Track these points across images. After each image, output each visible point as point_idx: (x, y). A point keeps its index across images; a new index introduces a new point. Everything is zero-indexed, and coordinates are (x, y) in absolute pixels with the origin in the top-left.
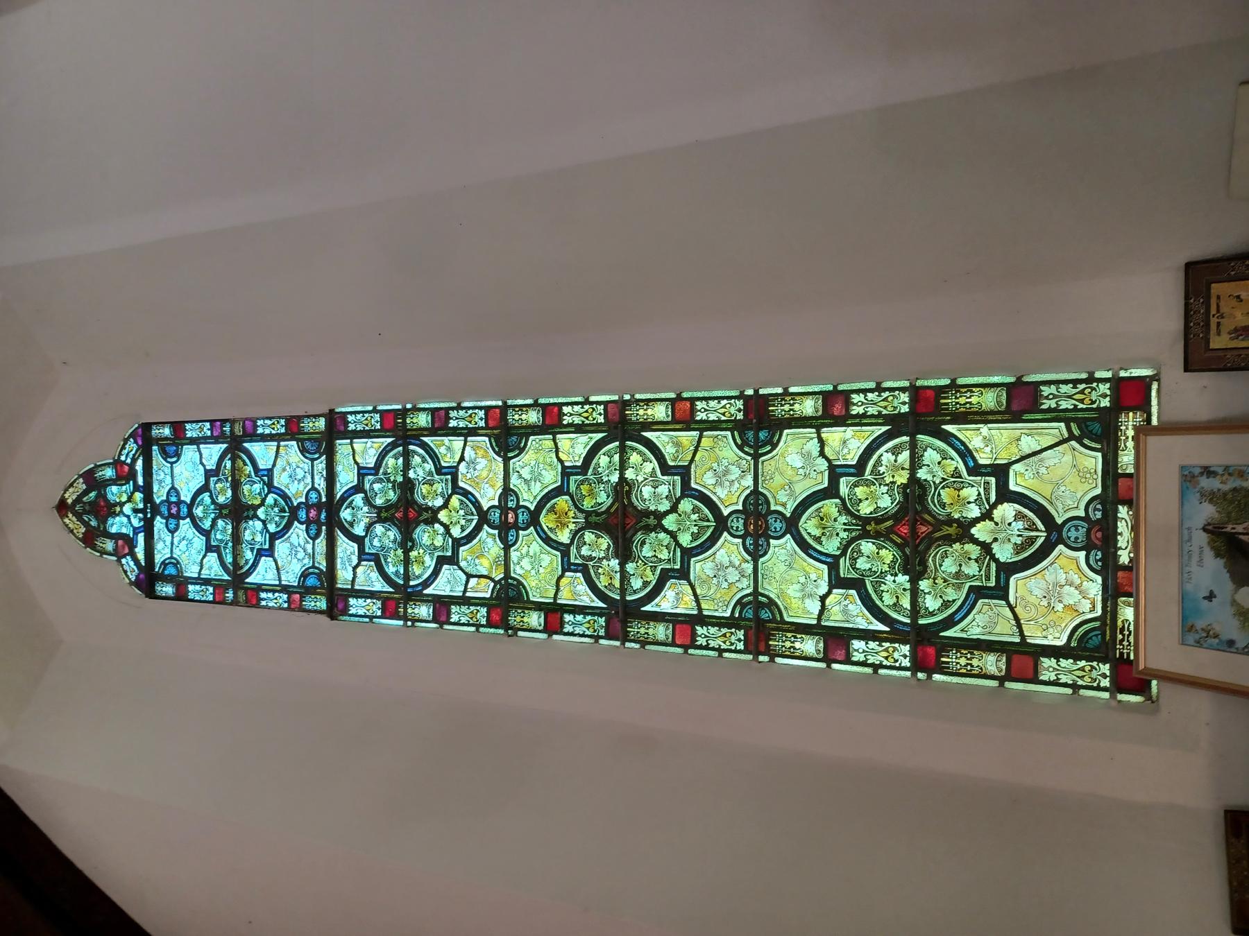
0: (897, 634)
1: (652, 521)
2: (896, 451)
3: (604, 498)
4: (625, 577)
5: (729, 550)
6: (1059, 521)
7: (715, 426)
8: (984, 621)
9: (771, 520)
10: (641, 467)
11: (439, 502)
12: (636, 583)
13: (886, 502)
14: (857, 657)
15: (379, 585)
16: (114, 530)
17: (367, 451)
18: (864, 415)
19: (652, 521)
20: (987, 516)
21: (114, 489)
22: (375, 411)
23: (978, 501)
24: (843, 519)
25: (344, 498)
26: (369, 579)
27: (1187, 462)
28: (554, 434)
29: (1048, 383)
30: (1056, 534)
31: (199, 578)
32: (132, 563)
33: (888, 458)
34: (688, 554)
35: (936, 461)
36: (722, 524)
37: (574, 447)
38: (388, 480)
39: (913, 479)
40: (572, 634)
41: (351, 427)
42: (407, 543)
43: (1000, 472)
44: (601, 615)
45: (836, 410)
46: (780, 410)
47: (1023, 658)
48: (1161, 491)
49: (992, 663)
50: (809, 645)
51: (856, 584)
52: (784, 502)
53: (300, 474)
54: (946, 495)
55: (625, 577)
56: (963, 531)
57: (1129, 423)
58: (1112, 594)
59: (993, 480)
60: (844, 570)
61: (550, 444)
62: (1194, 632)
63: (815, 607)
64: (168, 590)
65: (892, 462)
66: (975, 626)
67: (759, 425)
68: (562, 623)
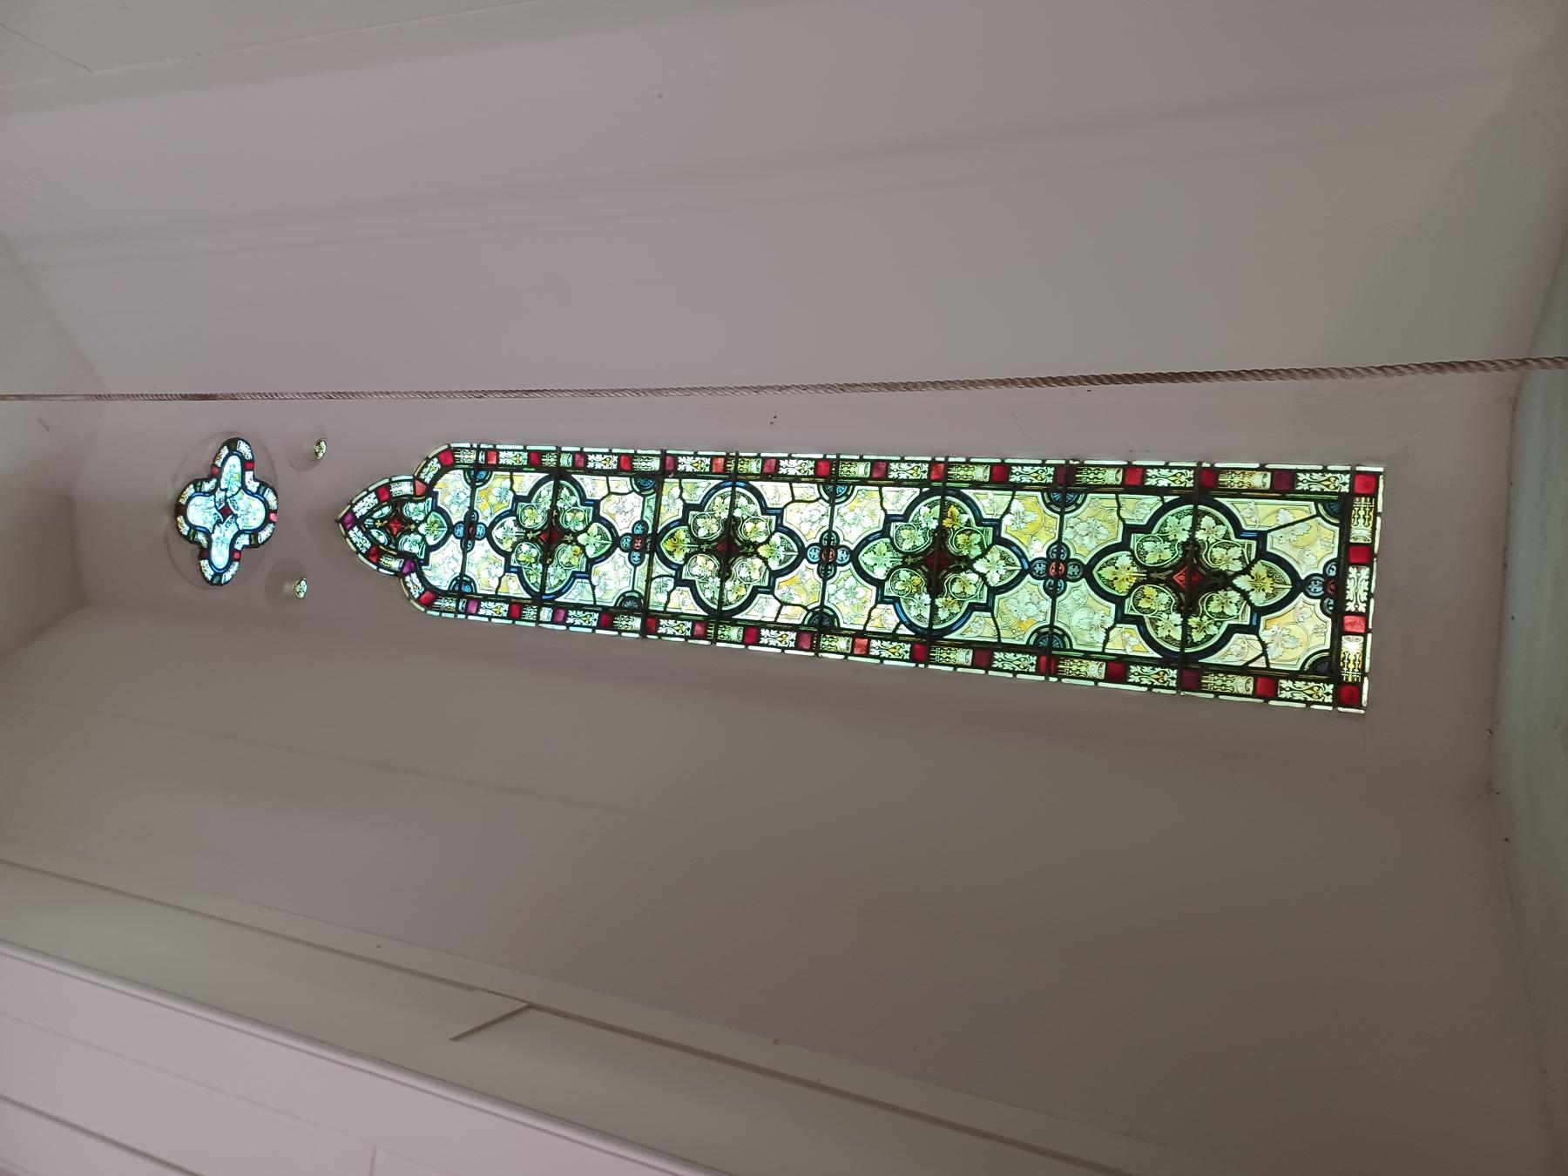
0: (1167, 659)
1: (1220, 581)
2: (931, 506)
3: (716, 530)
4: (934, 609)
5: (808, 573)
6: (1303, 577)
12: (942, 614)
14: (874, 652)
15: (691, 608)
16: (406, 548)
18: (1308, 492)
19: (909, 560)
20: (1246, 571)
21: (412, 506)
22: (525, 450)
23: (1242, 559)
26: (683, 601)
28: (880, 486)
30: (1300, 586)
31: (496, 596)
32: (417, 581)
33: (718, 500)
35: (1211, 530)
38: (1166, 539)
39: (1192, 538)
40: (767, 645)
43: (1261, 537)
46: (1086, 477)
47: (1267, 681)
50: (1095, 669)
51: (691, 584)
54: (569, 517)
55: (934, 609)
57: (1361, 505)
58: (1338, 633)
59: (1254, 543)
60: (889, 590)
61: (877, 495)
63: (495, 583)
65: (1178, 525)
67: (1065, 489)
68: (759, 636)
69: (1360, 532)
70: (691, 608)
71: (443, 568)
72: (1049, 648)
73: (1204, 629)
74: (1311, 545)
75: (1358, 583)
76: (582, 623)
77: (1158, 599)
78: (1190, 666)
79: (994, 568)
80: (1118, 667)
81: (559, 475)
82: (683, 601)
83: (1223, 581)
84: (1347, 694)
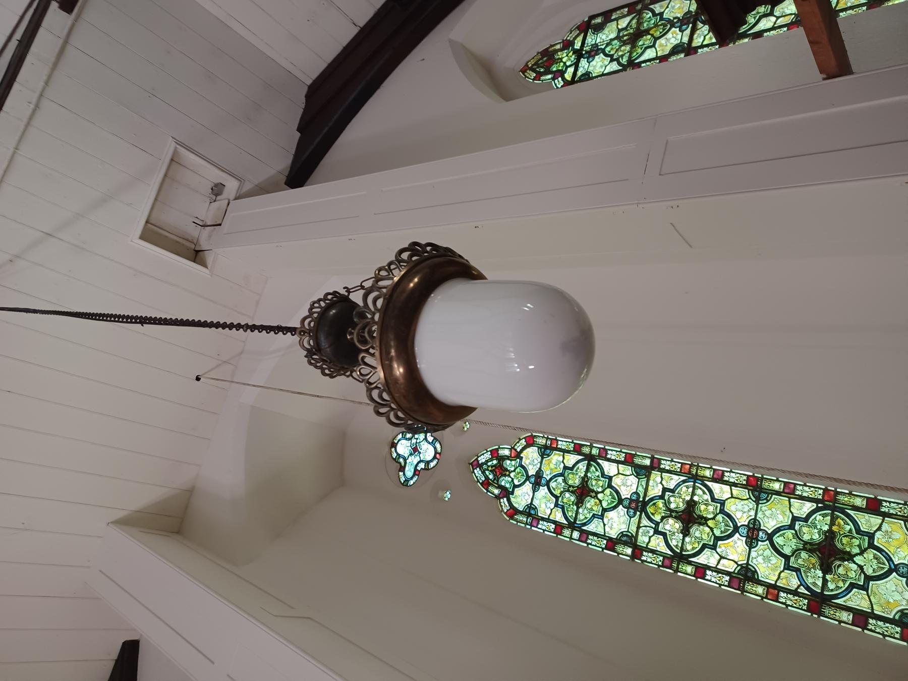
1: (808, 547)
2: (824, 516)
4: (825, 582)
7: (890, 515)
9: (761, 533)
11: (600, 490)
13: (816, 536)
17: (672, 481)
19: (703, 521)
20: (713, 518)
21: (508, 462)
23: (859, 546)
24: (795, 540)
25: (652, 499)
28: (790, 498)
29: (886, 501)
32: (506, 503)
33: (684, 489)
34: (718, 539)
36: (736, 529)
41: (609, 456)
44: (805, 598)
53: (536, 462)
55: (825, 582)
56: (850, 557)
63: (548, 512)
71: (522, 497)
82: (658, 543)
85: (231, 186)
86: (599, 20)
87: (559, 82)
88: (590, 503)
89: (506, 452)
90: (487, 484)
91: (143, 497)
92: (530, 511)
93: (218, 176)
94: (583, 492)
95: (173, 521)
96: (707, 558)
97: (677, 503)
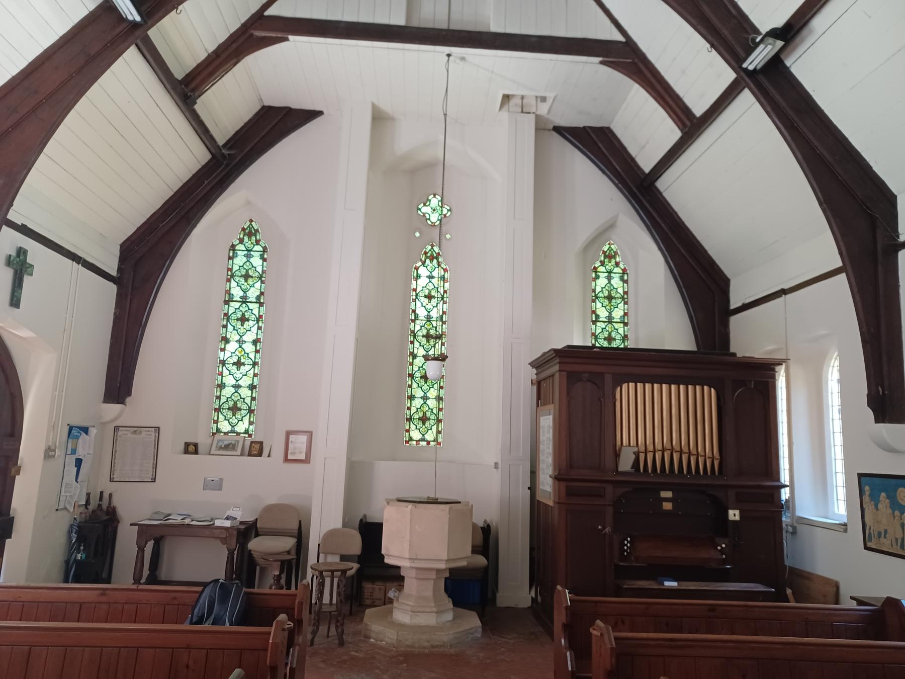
0: (220, 406)
8: (221, 418)
10: (247, 368)
17: (256, 312)
26: (418, 328)
27: (530, 361)
37: (252, 356)
42: (238, 319)
45: (253, 399)
47: (408, 431)
48: (238, 438)
49: (216, 418)
52: (240, 391)
62: (219, 441)
64: (231, 254)
65: (245, 407)
66: (220, 416)
69: (432, 443)
70: (230, 312)
71: (423, 271)
72: (412, 397)
73: (416, 422)
74: (430, 436)
75: (424, 443)
76: (412, 306)
77: (231, 404)
78: (410, 420)
79: (425, 387)
80: (409, 409)
81: (260, 277)
82: (418, 328)
83: (424, 424)
84: (407, 442)
85: (543, 109)
86: (626, 277)
87: (598, 264)
88: (426, 300)
89: (258, 237)
90: (426, 253)
91: (386, 106)
92: (418, 276)
93: (549, 102)
94: (247, 277)
95: (379, 118)
96: (417, 344)
97: (247, 315)
